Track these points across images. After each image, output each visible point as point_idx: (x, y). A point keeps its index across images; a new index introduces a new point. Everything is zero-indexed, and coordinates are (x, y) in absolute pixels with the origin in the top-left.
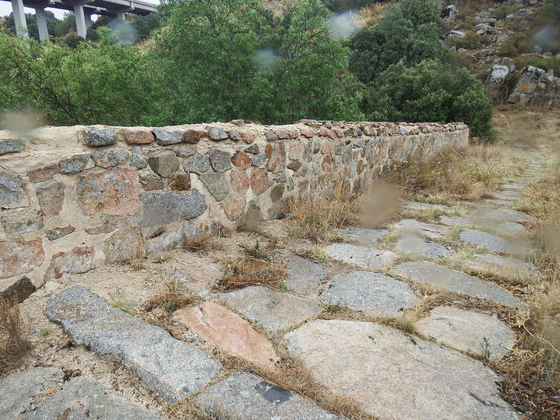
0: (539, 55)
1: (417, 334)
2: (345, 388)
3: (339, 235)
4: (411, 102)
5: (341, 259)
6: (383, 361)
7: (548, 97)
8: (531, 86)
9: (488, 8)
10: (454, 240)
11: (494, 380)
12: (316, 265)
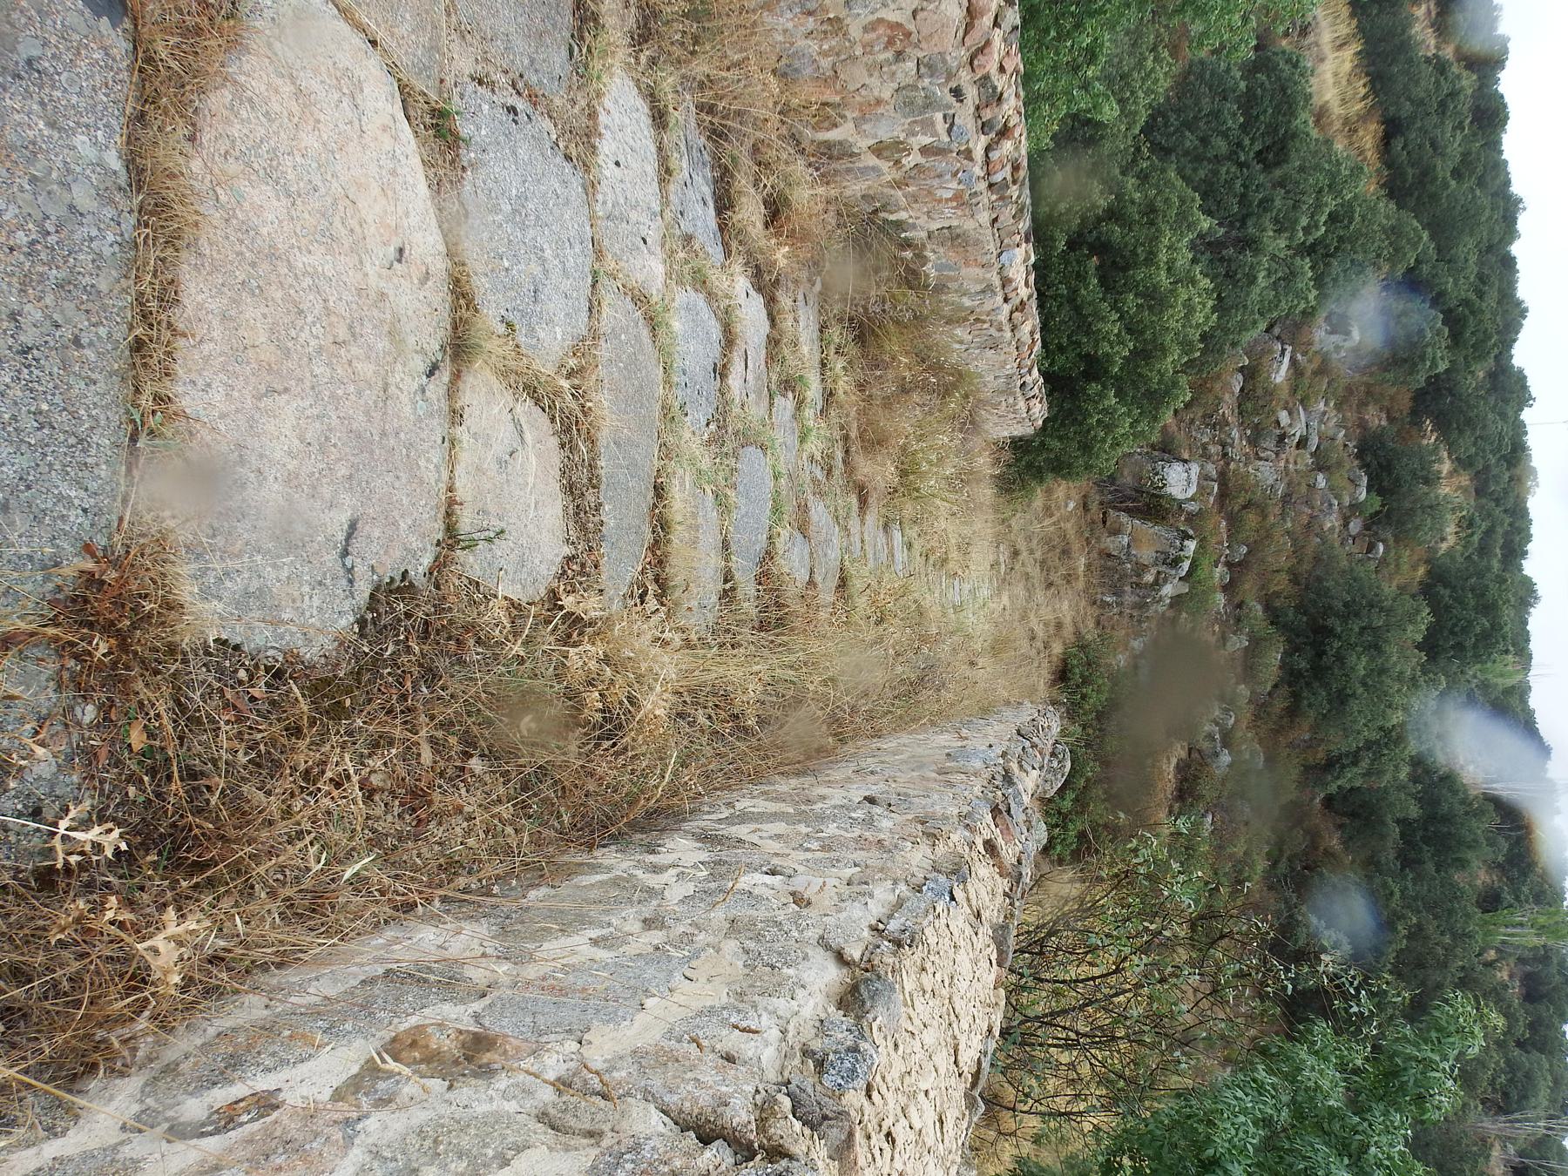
0: (1223, 559)
1: (457, 376)
2: (223, 198)
3: (675, 116)
4: (1092, 271)
5: (603, 131)
6: (347, 296)
7: (1124, 592)
8: (1146, 554)
9: (1344, 427)
10: (736, 434)
11: (409, 568)
12: (565, 53)
